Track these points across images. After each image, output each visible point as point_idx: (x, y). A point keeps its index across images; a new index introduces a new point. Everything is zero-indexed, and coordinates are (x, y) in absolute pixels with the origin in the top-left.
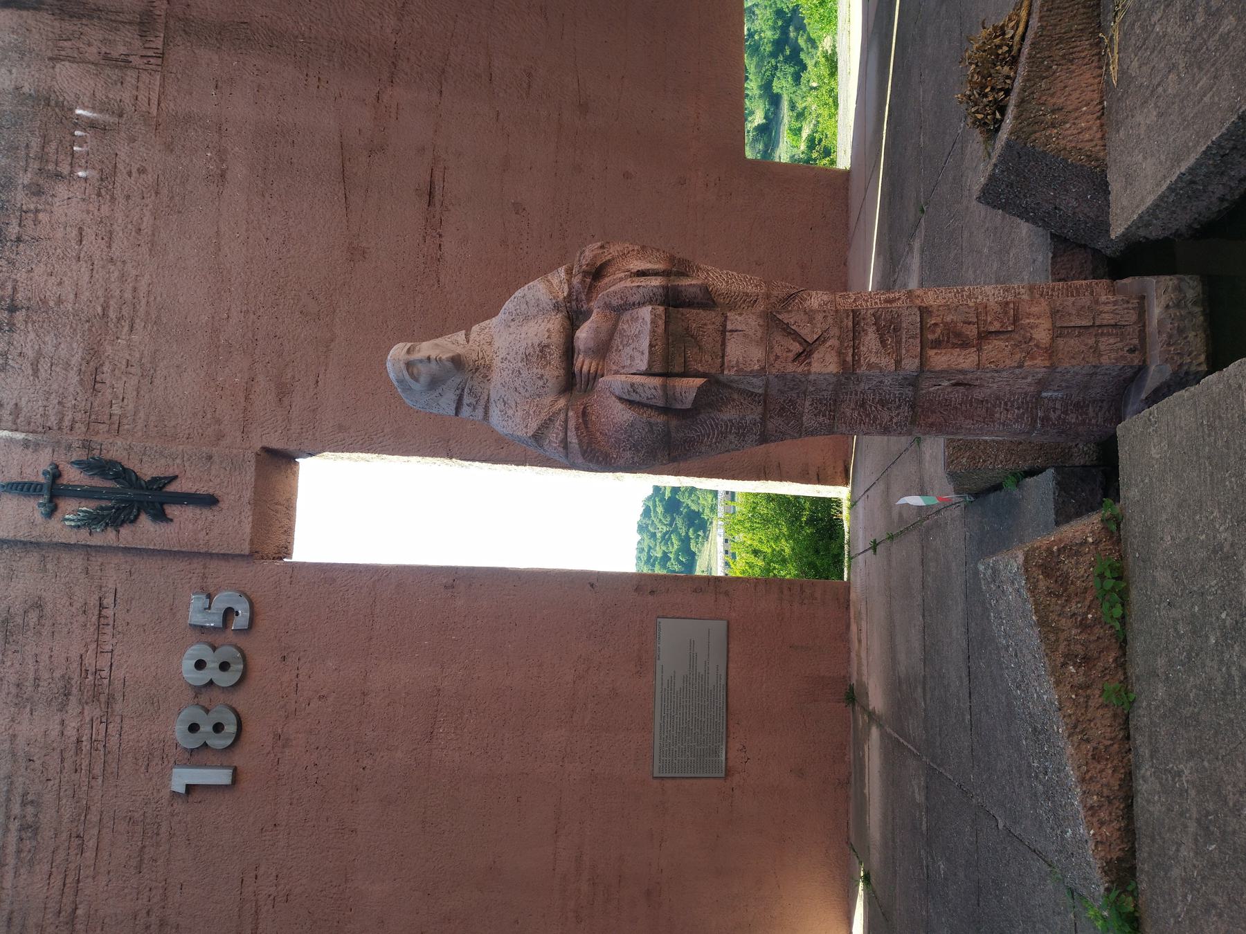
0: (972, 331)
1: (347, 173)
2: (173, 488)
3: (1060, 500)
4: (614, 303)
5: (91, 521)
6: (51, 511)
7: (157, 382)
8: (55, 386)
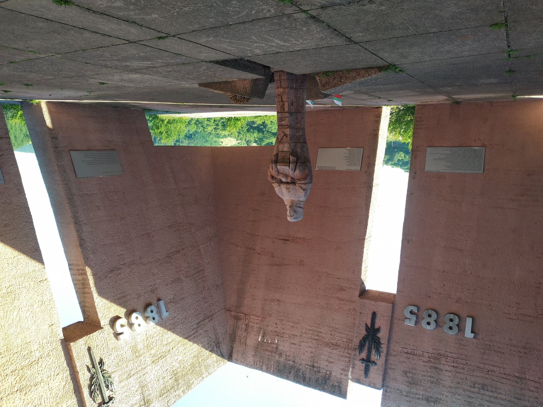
0: (281, 103)
2: (369, 325)
5: (378, 351)
6: (375, 363)
7: (337, 327)
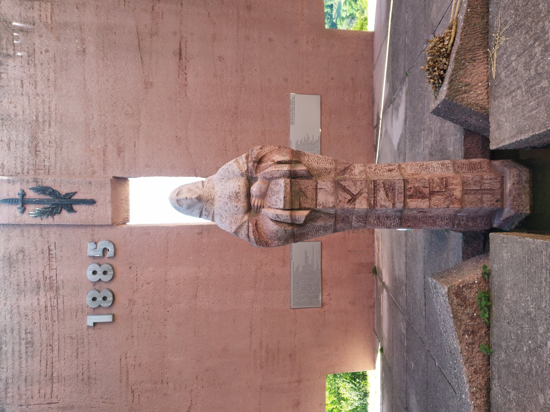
0: (426, 191)
1: (141, 47)
3: (465, 248)
4: (268, 177)
5: (42, 214)
6: (23, 210)
7: (63, 150)
8: (18, 154)
